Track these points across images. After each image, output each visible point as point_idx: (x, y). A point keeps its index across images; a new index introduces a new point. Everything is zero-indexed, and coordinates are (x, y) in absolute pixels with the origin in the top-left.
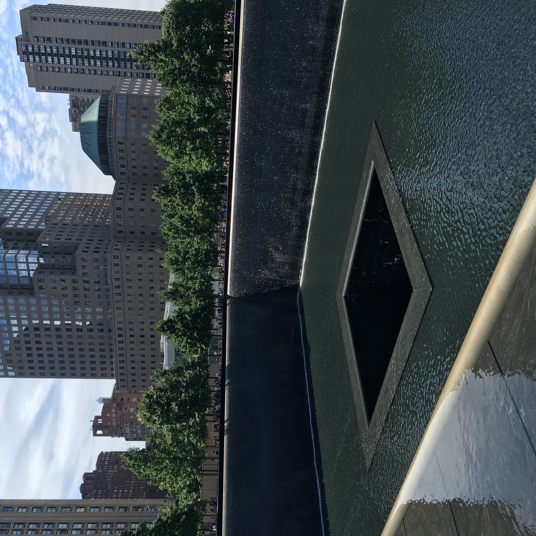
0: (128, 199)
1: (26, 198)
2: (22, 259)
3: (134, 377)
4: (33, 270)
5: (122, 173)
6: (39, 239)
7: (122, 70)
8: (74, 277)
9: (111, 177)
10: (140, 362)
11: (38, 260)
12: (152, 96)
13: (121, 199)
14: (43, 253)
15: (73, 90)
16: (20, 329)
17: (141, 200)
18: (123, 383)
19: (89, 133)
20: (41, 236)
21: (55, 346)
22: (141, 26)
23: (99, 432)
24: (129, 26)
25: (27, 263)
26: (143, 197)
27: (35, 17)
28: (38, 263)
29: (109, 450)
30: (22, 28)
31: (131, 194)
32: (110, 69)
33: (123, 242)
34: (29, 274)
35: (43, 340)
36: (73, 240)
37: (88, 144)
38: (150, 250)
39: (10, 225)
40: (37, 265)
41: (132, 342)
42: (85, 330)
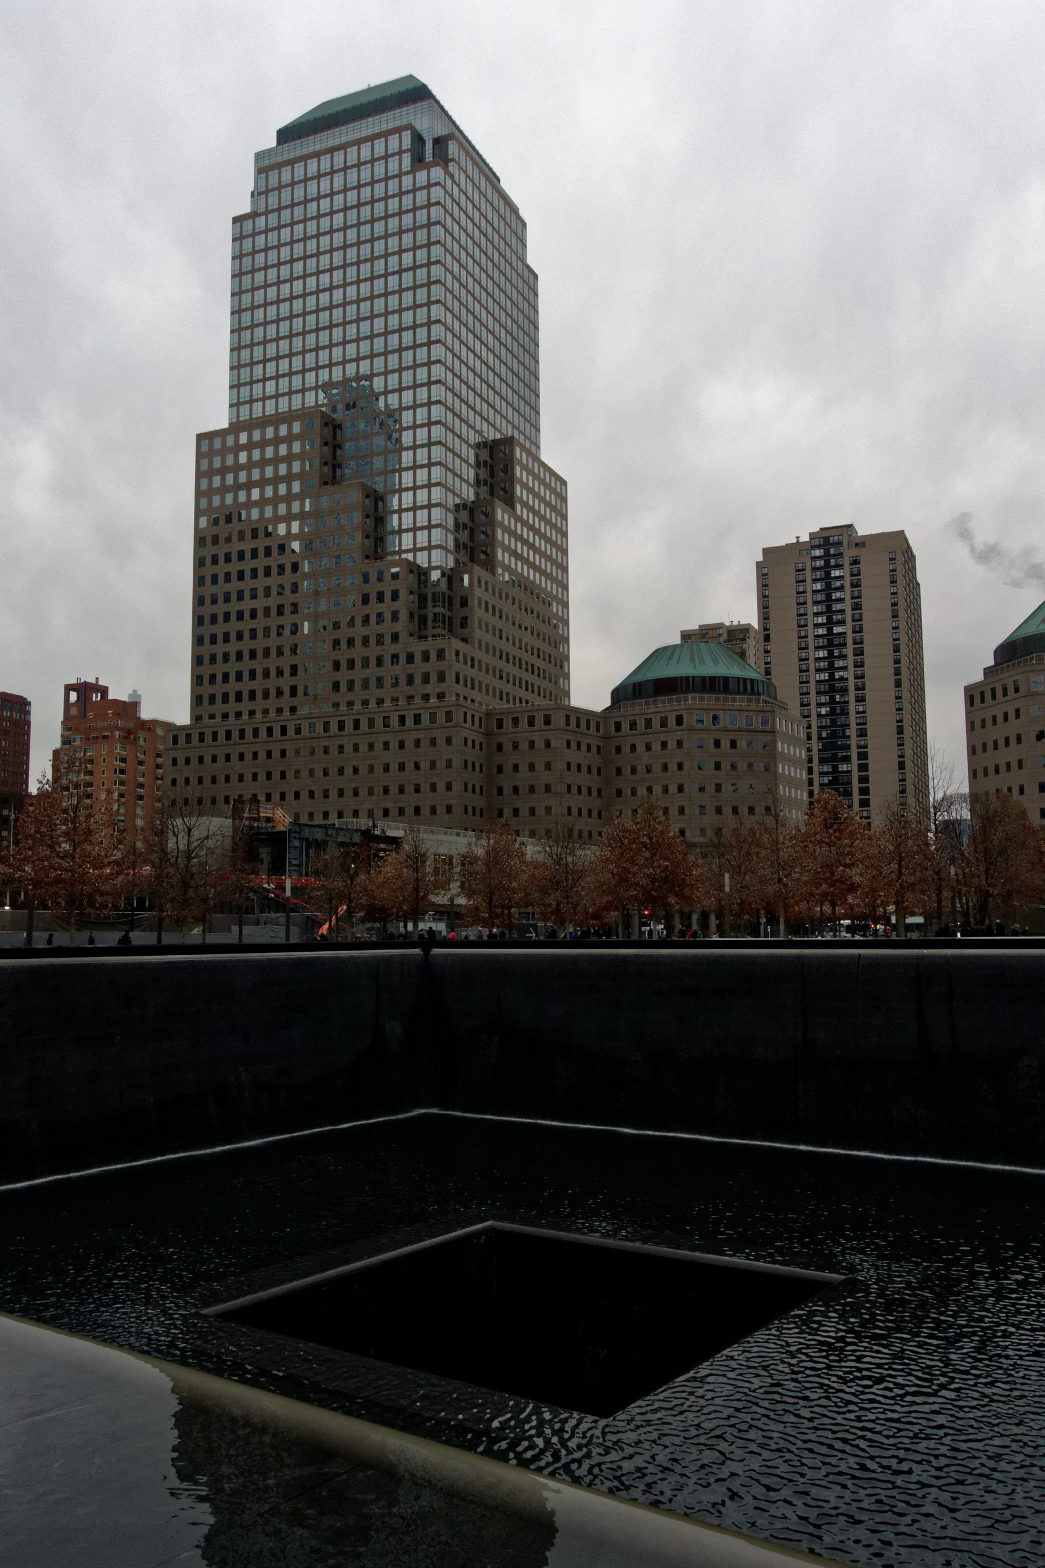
0: (569, 738)
1: (554, 562)
2: (437, 535)
3: (194, 761)
4: (415, 557)
5: (618, 727)
6: (478, 570)
7: (809, 575)
8: (403, 636)
9: (609, 704)
10: (227, 773)
11: (436, 568)
12: (776, 779)
13: (568, 724)
14: (451, 577)
15: (767, 638)
17: (569, 765)
18: (182, 740)
19: (692, 659)
20: (484, 572)
21: (259, 604)
22: (901, 721)
23: (73, 696)
24: (898, 721)
25: (430, 548)
26: (574, 768)
27: (895, 582)
28: (430, 568)
30: (872, 535)
31: (579, 744)
32: (812, 654)
33: (479, 730)
34: (408, 551)
35: (274, 581)
36: (478, 634)
37: (670, 658)
38: (466, 784)
39: (500, 514)
40: (425, 565)
41: (269, 755)
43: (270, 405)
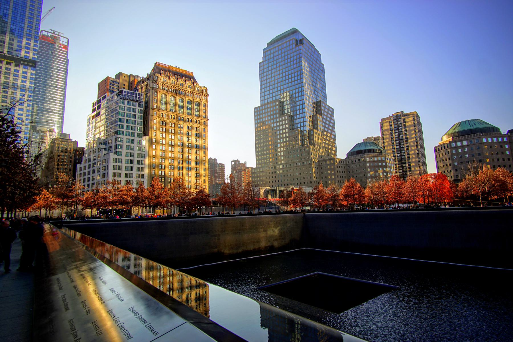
16: (278, 118)
19: (365, 146)
23: (233, 163)
26: (339, 172)
29: (226, 168)
31: (340, 166)
37: (360, 146)
42: (277, 157)
43: (266, 101)
